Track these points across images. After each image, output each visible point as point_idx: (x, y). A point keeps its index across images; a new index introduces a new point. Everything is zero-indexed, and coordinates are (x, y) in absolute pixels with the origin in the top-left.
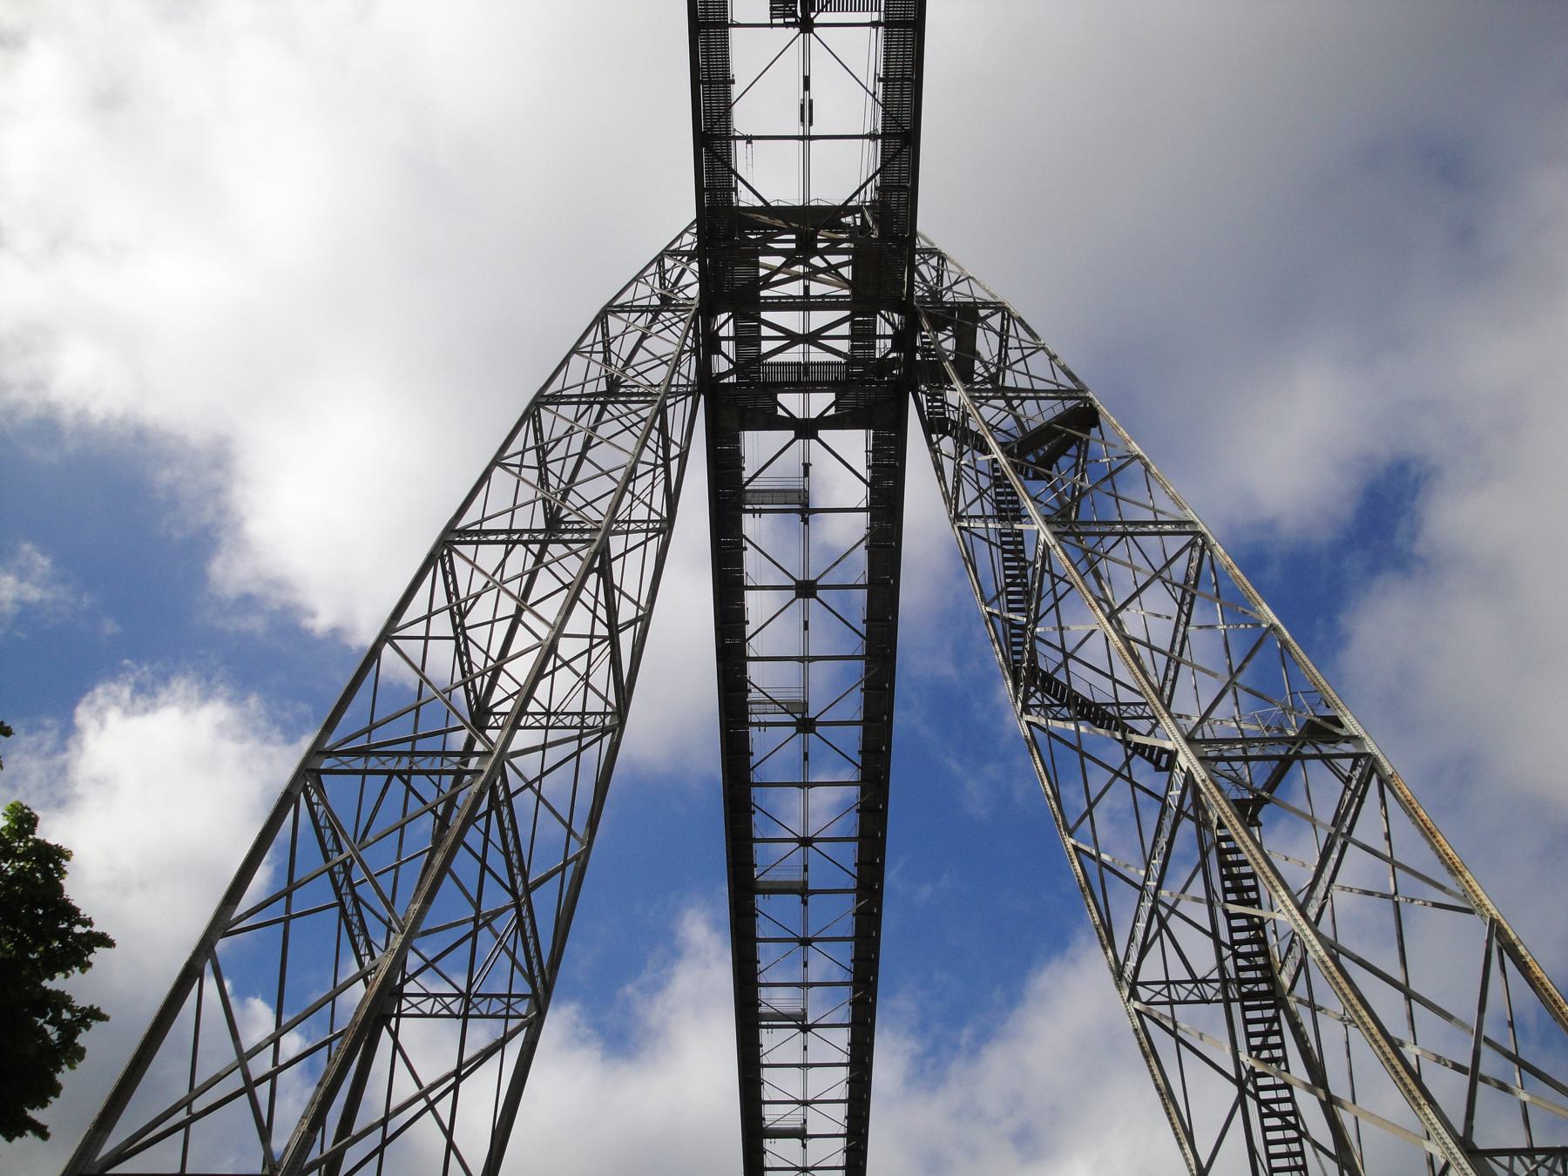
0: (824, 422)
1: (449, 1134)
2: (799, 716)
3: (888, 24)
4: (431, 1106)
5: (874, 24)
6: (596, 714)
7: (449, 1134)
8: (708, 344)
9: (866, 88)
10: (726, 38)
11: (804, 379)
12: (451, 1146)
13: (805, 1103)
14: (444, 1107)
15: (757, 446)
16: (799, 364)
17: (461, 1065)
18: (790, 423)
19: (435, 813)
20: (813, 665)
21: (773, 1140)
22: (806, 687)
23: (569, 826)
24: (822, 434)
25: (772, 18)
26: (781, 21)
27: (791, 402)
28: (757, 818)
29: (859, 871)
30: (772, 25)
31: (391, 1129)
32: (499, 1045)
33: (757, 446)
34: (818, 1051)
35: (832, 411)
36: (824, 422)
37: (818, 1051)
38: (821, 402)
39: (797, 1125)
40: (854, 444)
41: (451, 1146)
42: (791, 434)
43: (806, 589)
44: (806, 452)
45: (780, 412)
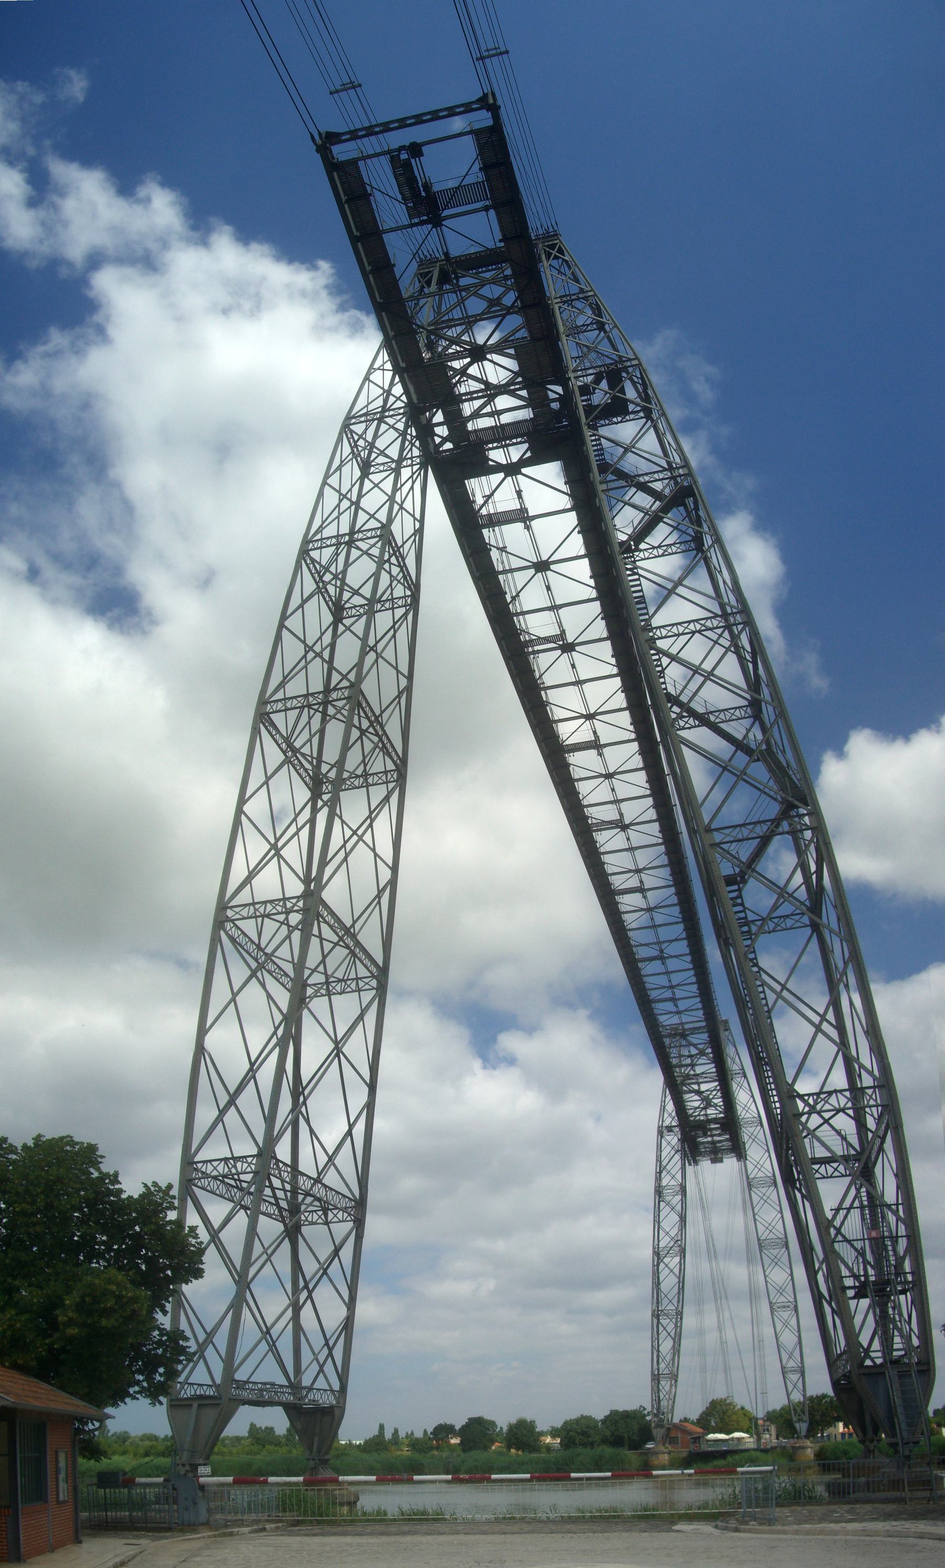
0: (524, 462)
1: (374, 850)
2: (561, 643)
3: (496, 206)
4: (360, 838)
5: (486, 209)
6: (400, 598)
7: (374, 850)
8: (425, 432)
9: (466, 175)
10: (382, 239)
11: (502, 435)
12: (376, 855)
13: (590, 717)
14: (368, 837)
15: (477, 487)
16: (492, 428)
17: (371, 813)
18: (498, 468)
19: (322, 657)
20: (637, 852)
21: (571, 754)
22: (560, 625)
23: (396, 668)
24: (524, 470)
25: (410, 219)
26: (416, 220)
27: (497, 455)
28: (494, 554)
29: (673, 878)
30: (412, 226)
31: (303, 662)
32: (387, 799)
33: (477, 487)
34: (636, 838)
35: (528, 454)
36: (524, 462)
37: (636, 838)
38: (516, 453)
39: (590, 737)
40: (551, 471)
41: (376, 855)
42: (502, 475)
43: (542, 566)
44: (516, 484)
45: (491, 463)
